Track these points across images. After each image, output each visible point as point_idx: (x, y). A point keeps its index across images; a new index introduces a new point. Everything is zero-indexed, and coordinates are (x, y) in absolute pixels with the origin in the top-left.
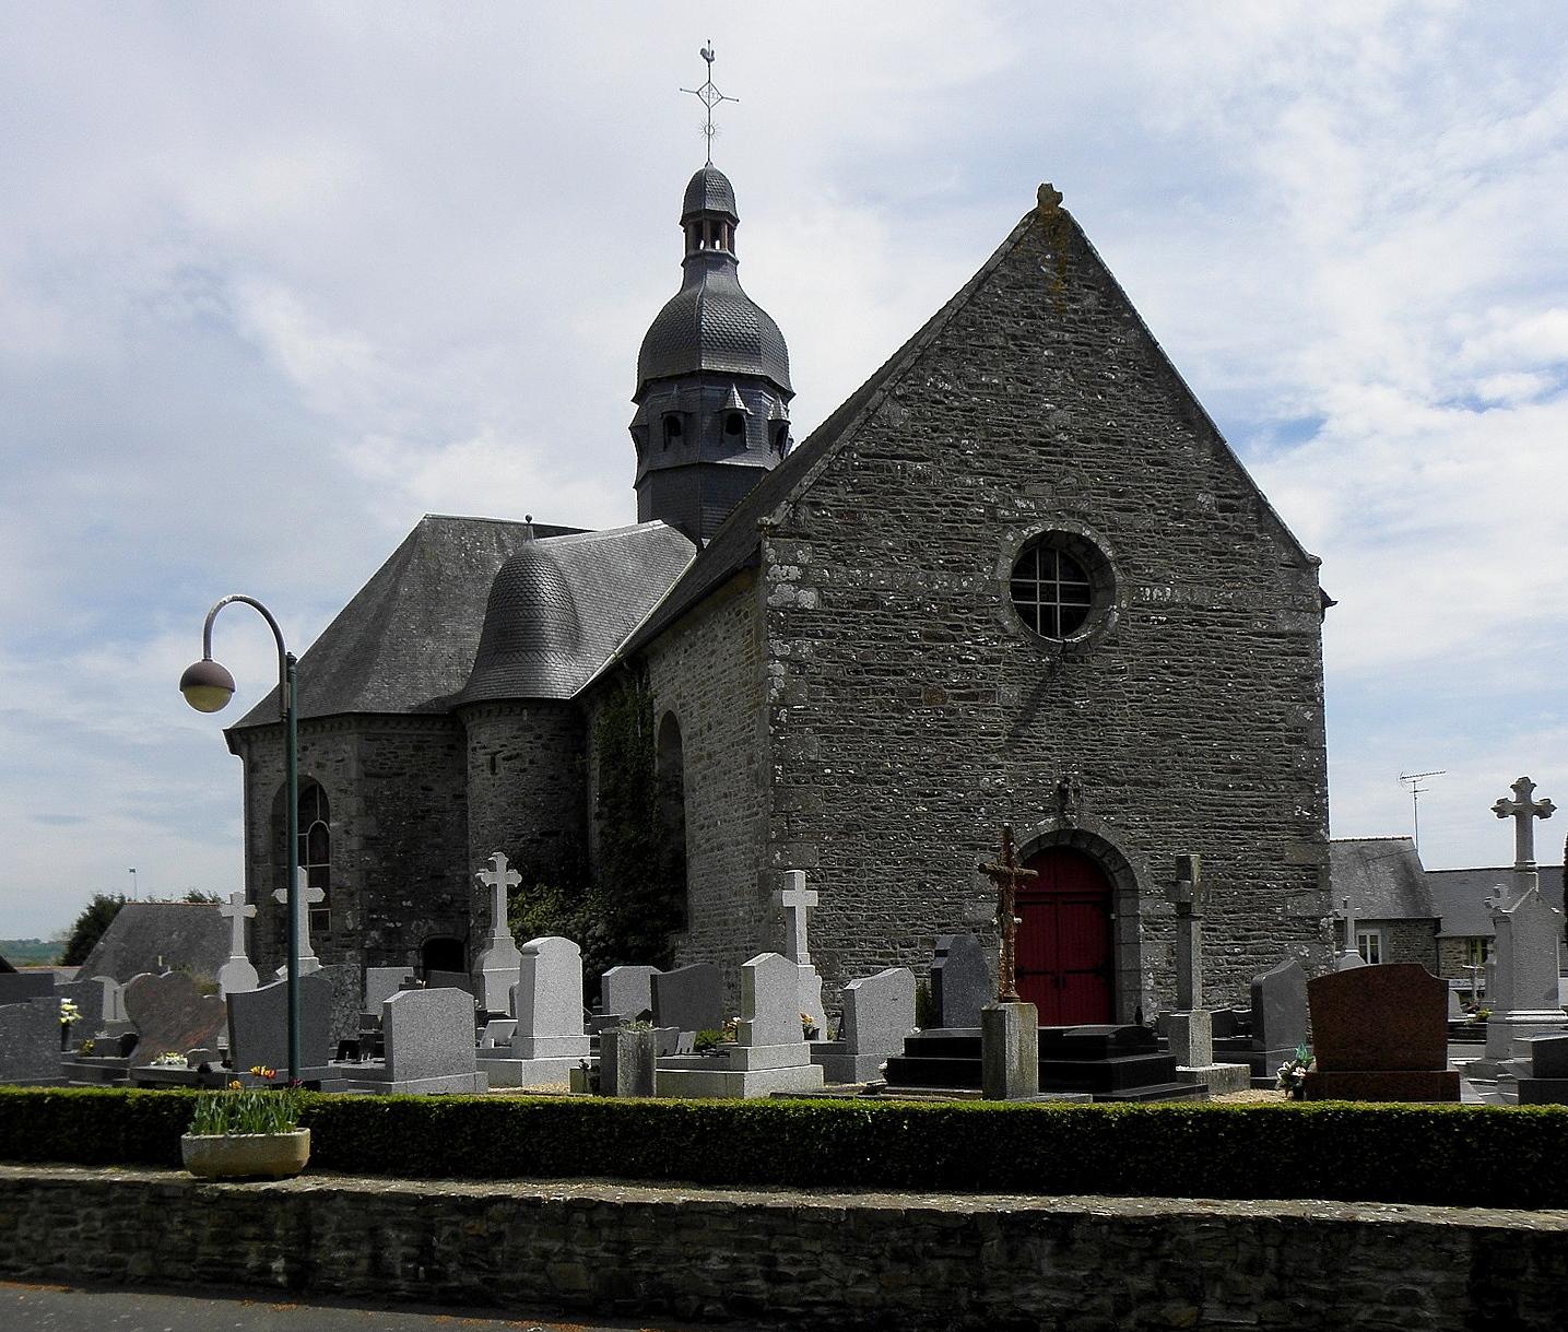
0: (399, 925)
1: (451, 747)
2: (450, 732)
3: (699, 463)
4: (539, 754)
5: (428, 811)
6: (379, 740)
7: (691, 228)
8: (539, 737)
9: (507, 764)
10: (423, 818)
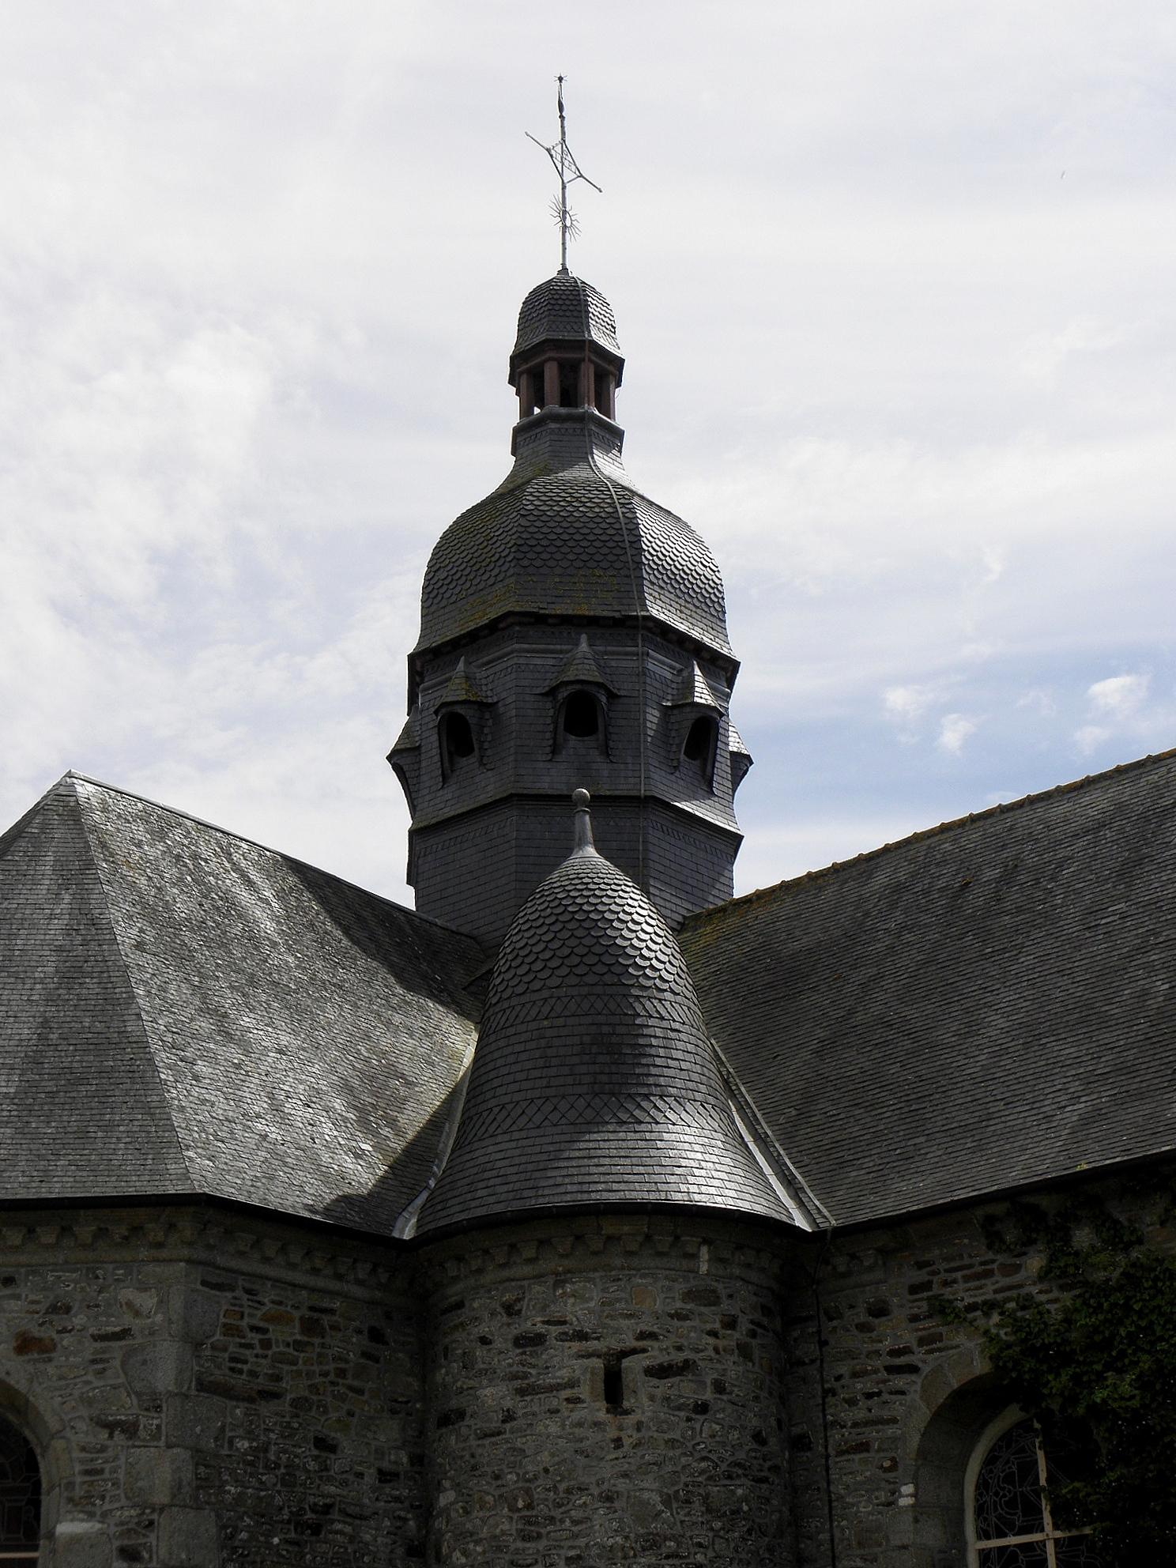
1: (376, 1335)
2: (378, 1294)
3: (646, 797)
4: (733, 1369)
5: (327, 1508)
6: (232, 1289)
7: (524, 380)
8: (731, 1323)
9: (662, 1387)
10: (316, 1530)
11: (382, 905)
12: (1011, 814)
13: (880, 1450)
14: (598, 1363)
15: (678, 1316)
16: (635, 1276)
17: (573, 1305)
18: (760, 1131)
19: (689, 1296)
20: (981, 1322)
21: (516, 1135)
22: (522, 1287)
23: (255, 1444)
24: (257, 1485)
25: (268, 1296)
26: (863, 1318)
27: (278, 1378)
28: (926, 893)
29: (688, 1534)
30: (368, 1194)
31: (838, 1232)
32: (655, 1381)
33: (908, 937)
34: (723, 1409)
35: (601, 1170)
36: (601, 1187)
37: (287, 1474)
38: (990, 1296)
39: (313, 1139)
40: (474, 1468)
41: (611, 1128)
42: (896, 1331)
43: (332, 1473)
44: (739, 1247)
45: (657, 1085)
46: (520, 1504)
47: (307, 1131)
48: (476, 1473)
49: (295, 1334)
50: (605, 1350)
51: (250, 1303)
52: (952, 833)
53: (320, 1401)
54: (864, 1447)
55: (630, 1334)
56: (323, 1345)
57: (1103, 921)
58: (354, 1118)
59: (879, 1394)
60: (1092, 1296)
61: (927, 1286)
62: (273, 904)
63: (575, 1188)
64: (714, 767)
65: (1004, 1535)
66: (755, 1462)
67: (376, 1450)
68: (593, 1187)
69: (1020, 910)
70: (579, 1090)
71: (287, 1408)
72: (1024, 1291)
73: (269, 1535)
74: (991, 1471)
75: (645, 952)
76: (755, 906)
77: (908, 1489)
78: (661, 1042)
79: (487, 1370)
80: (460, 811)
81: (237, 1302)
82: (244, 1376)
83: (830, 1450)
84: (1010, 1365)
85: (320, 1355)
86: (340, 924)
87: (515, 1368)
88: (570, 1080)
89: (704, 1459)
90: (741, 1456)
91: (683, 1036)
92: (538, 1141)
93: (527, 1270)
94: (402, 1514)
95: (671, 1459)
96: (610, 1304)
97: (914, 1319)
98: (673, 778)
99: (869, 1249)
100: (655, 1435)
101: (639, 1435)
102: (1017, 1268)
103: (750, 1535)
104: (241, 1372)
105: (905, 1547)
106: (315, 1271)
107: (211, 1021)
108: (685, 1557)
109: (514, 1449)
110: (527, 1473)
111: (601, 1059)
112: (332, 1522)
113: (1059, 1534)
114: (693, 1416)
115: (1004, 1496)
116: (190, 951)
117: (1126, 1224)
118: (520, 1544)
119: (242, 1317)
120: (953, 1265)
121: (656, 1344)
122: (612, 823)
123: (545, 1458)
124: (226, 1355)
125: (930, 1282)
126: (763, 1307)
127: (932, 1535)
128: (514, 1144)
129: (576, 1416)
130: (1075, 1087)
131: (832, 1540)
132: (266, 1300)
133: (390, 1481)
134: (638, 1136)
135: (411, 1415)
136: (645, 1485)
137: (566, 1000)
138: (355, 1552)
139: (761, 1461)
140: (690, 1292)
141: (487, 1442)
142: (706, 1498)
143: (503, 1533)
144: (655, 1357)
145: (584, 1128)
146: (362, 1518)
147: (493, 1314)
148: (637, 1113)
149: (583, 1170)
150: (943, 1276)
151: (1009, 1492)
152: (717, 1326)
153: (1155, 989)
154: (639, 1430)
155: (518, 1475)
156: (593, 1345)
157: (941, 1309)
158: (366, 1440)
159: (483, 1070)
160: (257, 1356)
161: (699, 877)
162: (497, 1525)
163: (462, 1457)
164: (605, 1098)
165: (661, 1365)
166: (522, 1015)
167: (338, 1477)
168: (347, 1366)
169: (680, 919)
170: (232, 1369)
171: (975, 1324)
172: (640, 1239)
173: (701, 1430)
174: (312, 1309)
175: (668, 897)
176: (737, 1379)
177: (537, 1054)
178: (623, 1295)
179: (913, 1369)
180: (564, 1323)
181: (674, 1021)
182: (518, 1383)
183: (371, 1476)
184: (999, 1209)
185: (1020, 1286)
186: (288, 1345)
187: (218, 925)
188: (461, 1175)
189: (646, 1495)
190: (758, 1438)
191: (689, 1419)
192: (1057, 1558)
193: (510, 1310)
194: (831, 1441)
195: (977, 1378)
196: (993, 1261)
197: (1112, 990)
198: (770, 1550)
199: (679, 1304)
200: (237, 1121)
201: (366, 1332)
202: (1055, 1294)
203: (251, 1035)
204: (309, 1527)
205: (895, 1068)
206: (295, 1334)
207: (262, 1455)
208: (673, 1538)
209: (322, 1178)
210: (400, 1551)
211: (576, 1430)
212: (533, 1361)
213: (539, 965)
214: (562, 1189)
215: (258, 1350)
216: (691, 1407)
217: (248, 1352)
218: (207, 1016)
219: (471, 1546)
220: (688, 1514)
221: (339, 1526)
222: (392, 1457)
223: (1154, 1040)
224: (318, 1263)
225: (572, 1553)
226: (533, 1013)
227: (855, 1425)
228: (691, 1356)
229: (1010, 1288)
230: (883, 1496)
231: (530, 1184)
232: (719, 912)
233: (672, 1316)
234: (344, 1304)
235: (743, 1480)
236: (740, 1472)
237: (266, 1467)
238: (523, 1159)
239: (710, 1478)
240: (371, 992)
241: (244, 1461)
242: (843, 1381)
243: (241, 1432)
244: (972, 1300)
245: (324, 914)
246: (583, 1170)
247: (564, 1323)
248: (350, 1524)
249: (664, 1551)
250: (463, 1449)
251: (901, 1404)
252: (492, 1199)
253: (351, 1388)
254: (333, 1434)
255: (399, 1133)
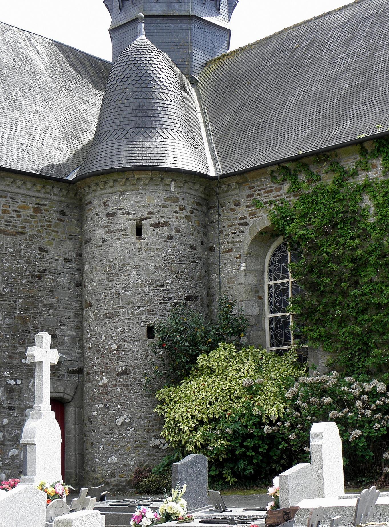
0: (19, 382)
1: (62, 213)
2: (63, 199)
3: (191, 16)
4: (183, 224)
5: (44, 271)
6: (5, 197)
8: (183, 209)
9: (156, 230)
10: (40, 278)
11: (93, 58)
12: (317, 20)
13: (235, 251)
14: (134, 222)
15: (163, 206)
16: (147, 192)
17: (126, 202)
18: (211, 140)
19: (167, 199)
20: (268, 208)
21: (108, 143)
22: (109, 196)
23: (15, 250)
24: (16, 263)
25: (20, 199)
26: (232, 206)
27: (24, 228)
28: (284, 51)
29: (164, 279)
30: (62, 164)
31: (223, 177)
32: (154, 228)
33: (274, 68)
34: (179, 238)
35: (135, 155)
36: (134, 161)
37: (28, 260)
38: (271, 199)
39: (43, 145)
40: (94, 258)
41: (141, 140)
42: (242, 211)
43: (46, 259)
44: (186, 182)
45: (159, 124)
46: (108, 270)
47: (41, 142)
48: (94, 259)
49: (30, 213)
50: (136, 218)
51: (13, 202)
52: (297, 28)
53: (41, 235)
54: (231, 250)
55: (145, 213)
56: (42, 216)
57: (335, 61)
58: (62, 137)
59: (236, 233)
60: (302, 199)
61: (252, 195)
62: (45, 59)
63: (126, 161)
64: (220, 3)
65: (277, 280)
66: (191, 255)
67: (63, 252)
68: (132, 161)
69: (311, 57)
70: (130, 126)
71: (28, 237)
72: (282, 197)
73: (22, 280)
74: (274, 259)
75: (158, 75)
76: (230, 56)
77: (244, 265)
78: (162, 109)
79: (98, 225)
80: (125, 22)
81: (8, 202)
82: (11, 227)
83: (221, 252)
84: (276, 223)
85: (40, 220)
86: (73, 66)
87: (106, 224)
88: (127, 123)
89: (170, 254)
90: (185, 254)
91: (170, 106)
92: (115, 145)
93: (110, 190)
94: (73, 273)
95: (159, 255)
96: (138, 202)
97: (248, 207)
98: (203, 8)
99: (234, 182)
100: (153, 247)
101: (148, 247)
102: (280, 189)
103: (187, 280)
104: (9, 225)
105: (242, 284)
106: (38, 191)
107: (10, 102)
108: (162, 287)
109: (106, 251)
110: (110, 259)
111: (139, 115)
112: (46, 275)
113: (293, 280)
114: (167, 240)
115: (277, 267)
116: (6, 77)
117: (316, 173)
118: (107, 283)
119: (10, 207)
120: (261, 188)
121: (154, 216)
122: (179, 26)
123: (115, 254)
124: (4, 220)
125: (253, 194)
126: (197, 203)
127: (252, 280)
128: (107, 146)
129: (126, 240)
130: (309, 124)
131: (220, 281)
132: (19, 201)
133: (68, 262)
134: (150, 143)
135: (77, 240)
136: (150, 263)
137: (128, 94)
138: (55, 285)
139: (193, 255)
140: (167, 198)
141: (98, 249)
142: (171, 268)
143: (102, 279)
144: (153, 220)
145: (131, 140)
146: (57, 274)
147: (100, 206)
148: (157, 134)
149: (129, 155)
150: (258, 192)
151: (279, 265)
152: (177, 209)
153: (344, 87)
154: (147, 245)
155: (107, 260)
156: (132, 216)
157: (257, 203)
158: (59, 248)
159: (102, 118)
160: (16, 220)
161: (213, 46)
162: (100, 277)
163: (90, 254)
164: (139, 129)
165: (156, 223)
166: (113, 99)
167: (48, 260)
168: (51, 223)
169: (205, 62)
170: (6, 225)
171: (267, 208)
172: (149, 179)
173: (170, 245)
174: (37, 204)
175: (200, 54)
176: (184, 228)
177: (117, 113)
178: (143, 199)
179: (247, 224)
180: (123, 208)
181: (168, 101)
182: (107, 229)
183: (61, 260)
184: (275, 168)
185: (281, 195)
186: (28, 216)
187: (20, 67)
188: (90, 157)
189: (149, 267)
190: (192, 247)
191: (165, 241)
192: (292, 288)
193: (105, 204)
194: (221, 248)
195: (266, 227)
196: (273, 187)
197: (331, 87)
198: (195, 285)
199: (163, 202)
200: (12, 138)
201: (59, 212)
202: (292, 198)
203: (25, 107)
204: (37, 277)
205: (257, 117)
206: (30, 213)
207: (18, 253)
208: (158, 281)
209: (43, 158)
210: (73, 285)
211: (126, 245)
212: (112, 222)
213: (119, 80)
214: (121, 162)
215: (16, 218)
216: (167, 237)
217: (12, 219)
218: (8, 100)
219: (93, 283)
220: (164, 273)
221: (49, 277)
222: (70, 254)
223: (338, 106)
224: (39, 188)
225: (124, 286)
226: (125, 97)
227: (228, 243)
228: (167, 220)
229: (278, 196)
230: (236, 267)
231: (111, 160)
232: (218, 59)
233: (160, 206)
234: (50, 202)
235: (185, 262)
236: (184, 259)
237: (20, 257)
238: (110, 151)
239: (172, 261)
240: (81, 91)
241: (11, 255)
242: (225, 228)
243: (10, 246)
244: (266, 200)
245: (67, 62)
246: (129, 155)
247: (123, 208)
248: (53, 276)
249: (155, 285)
250: (91, 251)
251: (243, 236)
252: (98, 166)
253: (53, 231)
254: (46, 246)
255: (80, 142)
